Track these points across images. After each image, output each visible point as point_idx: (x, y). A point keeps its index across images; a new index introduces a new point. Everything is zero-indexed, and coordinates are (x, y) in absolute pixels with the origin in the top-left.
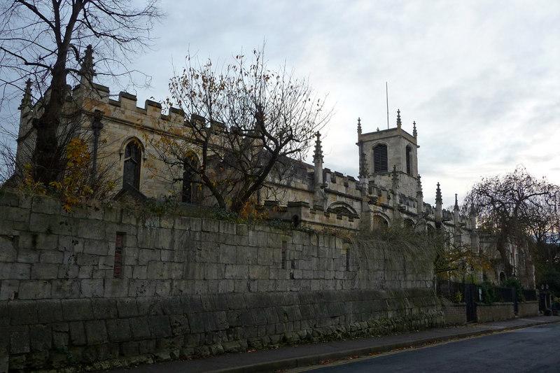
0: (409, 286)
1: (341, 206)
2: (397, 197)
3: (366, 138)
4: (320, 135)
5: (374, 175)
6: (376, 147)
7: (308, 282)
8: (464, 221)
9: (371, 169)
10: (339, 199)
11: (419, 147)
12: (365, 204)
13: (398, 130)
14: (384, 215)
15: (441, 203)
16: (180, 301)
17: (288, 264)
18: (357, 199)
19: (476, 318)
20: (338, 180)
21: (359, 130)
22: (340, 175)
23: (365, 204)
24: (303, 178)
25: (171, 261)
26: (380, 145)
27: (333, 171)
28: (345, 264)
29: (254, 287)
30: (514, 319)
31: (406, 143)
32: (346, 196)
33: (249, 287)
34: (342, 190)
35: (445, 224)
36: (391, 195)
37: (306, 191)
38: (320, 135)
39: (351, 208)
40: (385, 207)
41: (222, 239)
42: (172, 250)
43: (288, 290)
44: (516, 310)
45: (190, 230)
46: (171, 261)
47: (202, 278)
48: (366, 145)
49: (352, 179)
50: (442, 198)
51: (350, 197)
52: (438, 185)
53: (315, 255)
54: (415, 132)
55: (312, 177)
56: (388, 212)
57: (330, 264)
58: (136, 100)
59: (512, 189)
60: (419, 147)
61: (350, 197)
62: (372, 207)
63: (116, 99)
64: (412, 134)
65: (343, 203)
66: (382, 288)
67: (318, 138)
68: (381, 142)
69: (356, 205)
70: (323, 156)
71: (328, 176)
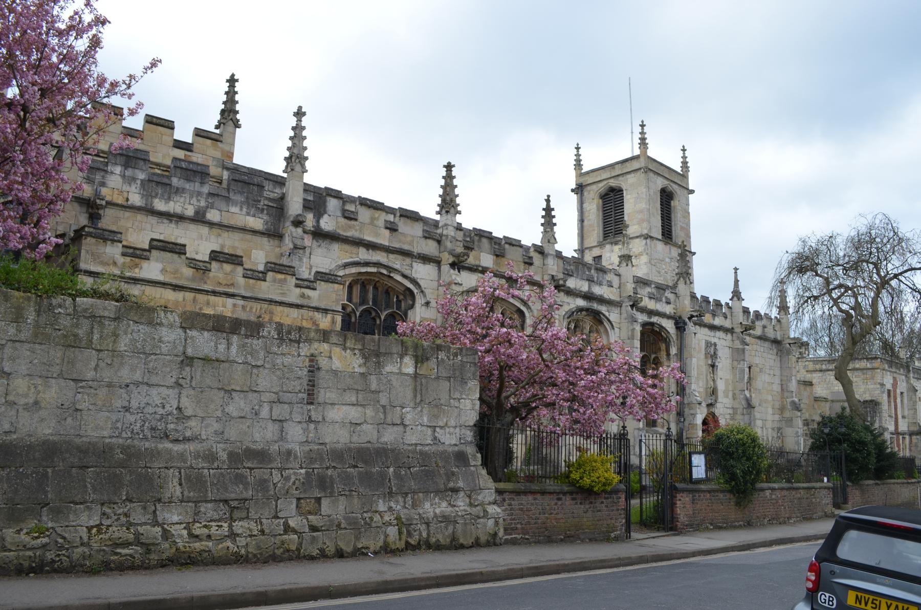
1: (374, 270)
2: (551, 262)
4: (304, 114)
5: (601, 245)
6: (606, 194)
9: (595, 234)
10: (363, 254)
11: (692, 192)
12: (445, 268)
13: (642, 159)
18: (425, 259)
19: (674, 519)
21: (578, 164)
23: (445, 268)
31: (660, 183)
32: (388, 250)
34: (384, 238)
37: (262, 233)
38: (304, 114)
54: (685, 164)
55: (279, 208)
58: (173, 128)
60: (692, 192)
63: (188, 138)
64: (679, 170)
65: (377, 264)
66: (351, 442)
68: (613, 183)
70: (307, 158)
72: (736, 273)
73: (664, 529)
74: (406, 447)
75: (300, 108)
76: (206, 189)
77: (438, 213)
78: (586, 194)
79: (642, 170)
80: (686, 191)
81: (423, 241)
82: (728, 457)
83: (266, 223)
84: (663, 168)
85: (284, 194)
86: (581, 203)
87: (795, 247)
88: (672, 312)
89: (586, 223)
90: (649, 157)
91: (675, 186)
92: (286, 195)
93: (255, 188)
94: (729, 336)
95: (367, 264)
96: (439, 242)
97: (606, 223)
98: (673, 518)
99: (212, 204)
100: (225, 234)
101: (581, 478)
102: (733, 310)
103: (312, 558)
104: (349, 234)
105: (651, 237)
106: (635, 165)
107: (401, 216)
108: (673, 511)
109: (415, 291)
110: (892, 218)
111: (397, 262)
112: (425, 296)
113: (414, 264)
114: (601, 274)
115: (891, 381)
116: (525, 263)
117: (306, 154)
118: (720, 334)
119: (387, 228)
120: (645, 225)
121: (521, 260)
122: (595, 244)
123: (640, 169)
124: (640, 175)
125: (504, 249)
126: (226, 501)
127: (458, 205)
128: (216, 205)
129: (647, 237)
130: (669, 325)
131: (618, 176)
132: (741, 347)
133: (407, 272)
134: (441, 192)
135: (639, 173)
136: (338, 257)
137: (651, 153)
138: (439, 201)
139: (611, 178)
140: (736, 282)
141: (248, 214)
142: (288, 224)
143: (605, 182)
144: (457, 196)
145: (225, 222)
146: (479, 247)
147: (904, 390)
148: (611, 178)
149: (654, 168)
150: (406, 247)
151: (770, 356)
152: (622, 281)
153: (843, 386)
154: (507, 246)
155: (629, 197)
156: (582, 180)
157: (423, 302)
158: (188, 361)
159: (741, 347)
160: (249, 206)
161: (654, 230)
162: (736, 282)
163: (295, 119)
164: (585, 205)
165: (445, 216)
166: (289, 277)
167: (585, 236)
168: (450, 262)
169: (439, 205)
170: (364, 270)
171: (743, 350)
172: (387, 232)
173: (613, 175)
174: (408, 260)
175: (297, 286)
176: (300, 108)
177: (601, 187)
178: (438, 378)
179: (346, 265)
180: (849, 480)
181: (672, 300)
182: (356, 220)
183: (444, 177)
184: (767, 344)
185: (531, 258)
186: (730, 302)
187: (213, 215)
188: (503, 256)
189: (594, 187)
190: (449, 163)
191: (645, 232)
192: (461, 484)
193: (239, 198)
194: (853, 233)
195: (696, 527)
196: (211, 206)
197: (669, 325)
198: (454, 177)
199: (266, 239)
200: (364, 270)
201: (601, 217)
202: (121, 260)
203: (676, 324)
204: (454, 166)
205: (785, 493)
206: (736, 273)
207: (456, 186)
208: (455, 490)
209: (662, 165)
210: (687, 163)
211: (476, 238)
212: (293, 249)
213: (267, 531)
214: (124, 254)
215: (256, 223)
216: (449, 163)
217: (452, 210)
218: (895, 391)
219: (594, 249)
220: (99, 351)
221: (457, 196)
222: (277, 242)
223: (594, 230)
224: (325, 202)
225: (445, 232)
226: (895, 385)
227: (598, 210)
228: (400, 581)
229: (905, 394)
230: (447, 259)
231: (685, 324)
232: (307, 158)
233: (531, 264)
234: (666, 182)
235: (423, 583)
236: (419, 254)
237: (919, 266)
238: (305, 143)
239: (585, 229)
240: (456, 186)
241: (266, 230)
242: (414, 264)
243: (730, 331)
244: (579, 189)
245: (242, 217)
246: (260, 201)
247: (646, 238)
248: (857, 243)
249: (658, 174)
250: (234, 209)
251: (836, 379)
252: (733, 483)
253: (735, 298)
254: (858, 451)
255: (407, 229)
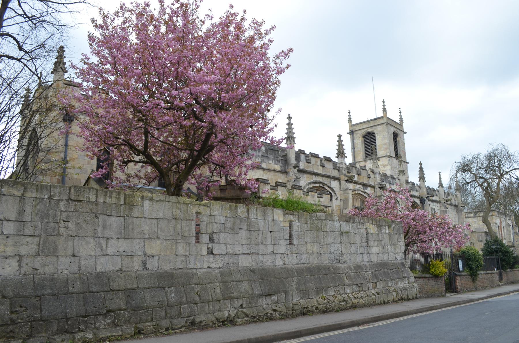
0: (375, 259)
2: (377, 176)
3: (357, 128)
4: (291, 118)
5: (365, 161)
6: (366, 135)
7: (236, 257)
8: (449, 198)
9: (361, 156)
10: (315, 178)
11: (405, 133)
12: (343, 182)
13: (385, 119)
14: (365, 193)
15: (424, 181)
16: (34, 281)
17: (205, 238)
18: (335, 179)
19: (456, 287)
20: (313, 160)
21: (350, 120)
22: (316, 156)
23: (343, 182)
24: (276, 159)
25: (20, 234)
26: (369, 133)
27: (307, 152)
28: (287, 236)
29: (152, 264)
30: (499, 286)
31: (393, 130)
32: (323, 176)
33: (144, 264)
34: (320, 171)
35: (429, 200)
36: (372, 175)
37: (278, 171)
38: (291, 118)
39: (329, 187)
40: (365, 185)
41: (100, 209)
42: (20, 221)
43: (206, 266)
44: (501, 279)
45: (50, 198)
46: (20, 234)
47: (70, 253)
48: (357, 134)
49: (328, 159)
50: (425, 176)
51: (328, 177)
52: (421, 164)
53: (245, 227)
54: (401, 119)
55: (285, 160)
56: (369, 190)
57: (266, 238)
59: (493, 166)
60: (405, 133)
61: (328, 177)
62: (351, 186)
64: (398, 122)
67: (290, 121)
68: (370, 130)
69: (334, 184)
70: (295, 138)
71: (302, 157)
72: (440, 174)
73: (453, 292)
74: (390, 262)
75: (289, 115)
76: (260, 154)
77: (337, 157)
78: (355, 135)
79: (385, 124)
80: (403, 133)
81: (333, 171)
82: (468, 261)
83: (281, 167)
84: (393, 122)
85: (286, 154)
86: (353, 139)
87: (460, 160)
88: (419, 195)
89: (356, 149)
90: (388, 117)
91: (398, 131)
92: (288, 154)
93: (276, 152)
94: (439, 205)
95: (316, 183)
96: (339, 170)
97: (366, 150)
98: (455, 287)
99: (263, 160)
100: (268, 173)
101: (435, 271)
102: (440, 192)
103: (379, 305)
104: (308, 170)
105: (391, 157)
106: (381, 121)
107: (325, 160)
108: (455, 284)
109: (332, 193)
110: (506, 146)
111: (325, 180)
112: (336, 195)
113: (331, 181)
114: (393, 179)
115: (499, 222)
116: (368, 177)
117: (294, 136)
118: (435, 204)
119: (321, 166)
120: (388, 151)
121: (366, 176)
122: (362, 160)
123: (384, 123)
124: (384, 126)
125: (360, 172)
126: (357, 284)
127: (345, 153)
128: (264, 160)
129: (390, 157)
130: (418, 201)
131: (372, 126)
132: (444, 209)
133: (329, 185)
134: (337, 148)
135: (383, 125)
136: (306, 181)
137: (388, 115)
138: (337, 152)
139: (368, 127)
140: (440, 179)
141: (275, 164)
142: (291, 167)
143: (366, 130)
144: (345, 149)
145: (268, 168)
146: (352, 172)
147: (504, 226)
148: (368, 127)
149: (390, 123)
150: (328, 174)
151: (454, 213)
152: (401, 182)
153: (487, 225)
154: (361, 170)
155: (378, 137)
156: (353, 128)
157: (336, 198)
158: (342, 233)
159: (444, 209)
160: (275, 161)
161: (392, 153)
162: (440, 179)
163: (288, 120)
164: (355, 141)
165: (340, 159)
166: (315, 193)
167: (356, 156)
168: (346, 179)
169: (337, 154)
170: (315, 185)
171: (446, 211)
172: (321, 167)
173: (369, 126)
174: (329, 180)
175: (318, 197)
176: (289, 115)
177: (364, 132)
178: (394, 234)
179: (310, 183)
180: (502, 269)
181: (418, 190)
182: (311, 163)
183: (338, 141)
184: (452, 207)
185: (369, 175)
186: (438, 189)
187: (264, 165)
188: (360, 175)
189: (359, 132)
190: (339, 135)
191: (388, 154)
192: (406, 275)
193: (271, 157)
194: (487, 153)
195: (463, 291)
196: (263, 161)
197: (418, 201)
198: (342, 141)
199: (282, 174)
200: (315, 185)
201: (364, 147)
202: (270, 191)
203: (421, 200)
204: (342, 136)
205: (485, 275)
206: (440, 174)
207: (344, 145)
208: (405, 278)
209: (393, 121)
210: (402, 118)
211: (351, 167)
212: (296, 179)
213: (368, 295)
214: (271, 189)
215: (278, 167)
216: (339, 135)
217: (343, 156)
218: (501, 226)
219: (361, 163)
220: (323, 232)
221: (345, 149)
222: (285, 175)
223: (360, 153)
224: (300, 156)
225: (341, 166)
226: (501, 223)
227: (362, 143)
228: (421, 309)
229: (505, 228)
230: (343, 178)
231: (425, 200)
232: (295, 138)
233: (370, 178)
234: (395, 129)
235: (425, 310)
236: (333, 177)
237: (518, 167)
238: (293, 131)
239: (356, 152)
240: (344, 145)
241: (282, 170)
242: (331, 181)
243: (439, 202)
244: (352, 133)
245: (273, 165)
246: (278, 158)
247: (389, 157)
248: (491, 157)
249: (392, 125)
250: (270, 162)
251: (483, 222)
252: (472, 272)
253: (440, 187)
254: (505, 256)
255: (329, 166)
